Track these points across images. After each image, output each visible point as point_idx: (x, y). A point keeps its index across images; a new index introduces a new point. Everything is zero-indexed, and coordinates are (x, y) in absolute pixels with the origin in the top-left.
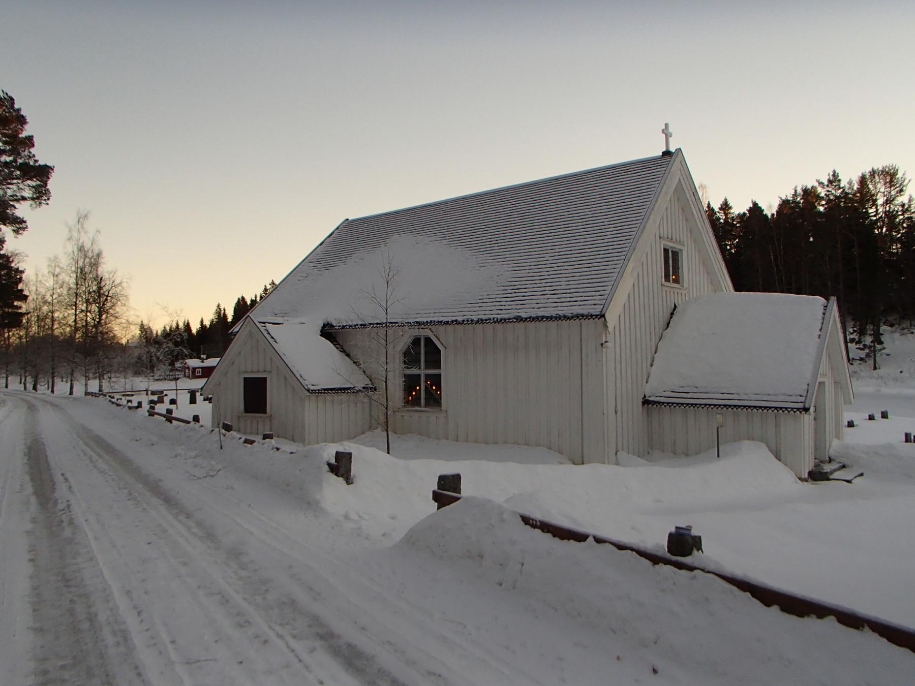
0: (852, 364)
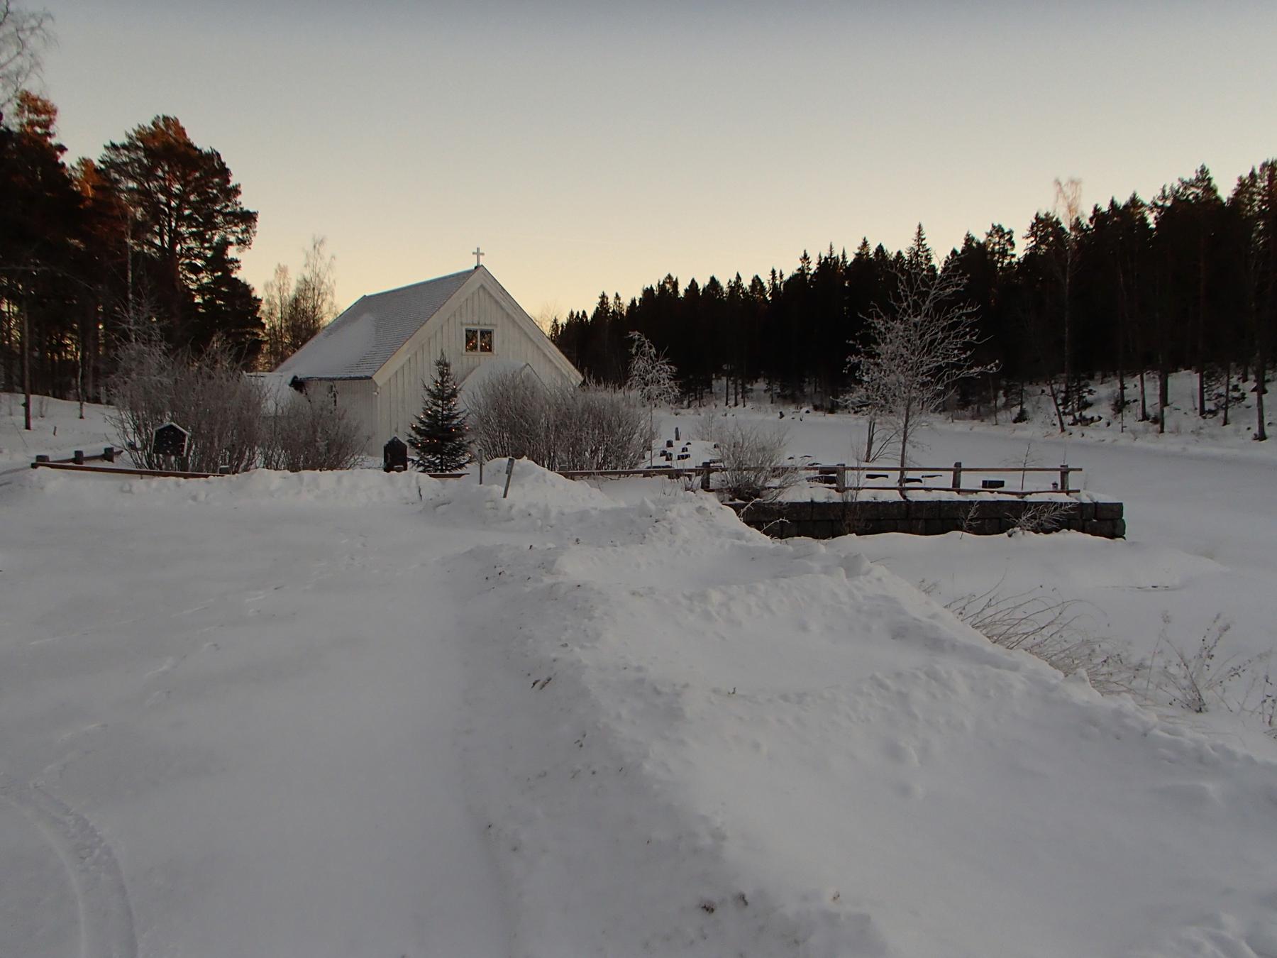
0: (1204, 418)
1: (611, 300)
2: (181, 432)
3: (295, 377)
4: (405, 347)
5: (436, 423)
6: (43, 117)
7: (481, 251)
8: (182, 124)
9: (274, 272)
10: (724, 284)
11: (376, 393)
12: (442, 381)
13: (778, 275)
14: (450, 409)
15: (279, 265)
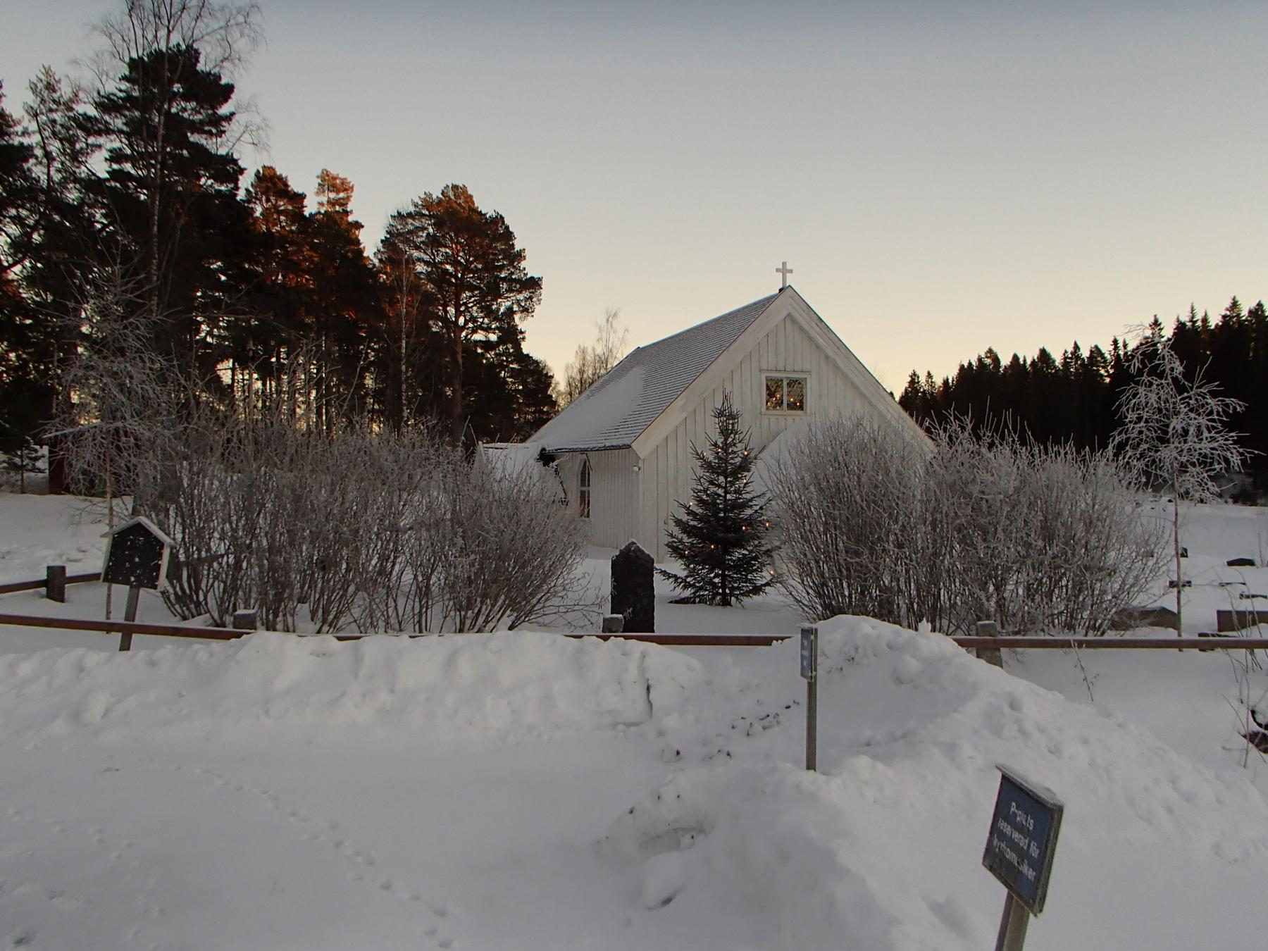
1: (923, 379)
2: (156, 539)
3: (543, 449)
4: (680, 402)
5: (715, 514)
6: (342, 195)
7: (788, 267)
9: (575, 353)
10: (1058, 359)
11: (636, 469)
12: (725, 443)
13: (1120, 344)
14: (738, 492)
15: (579, 347)
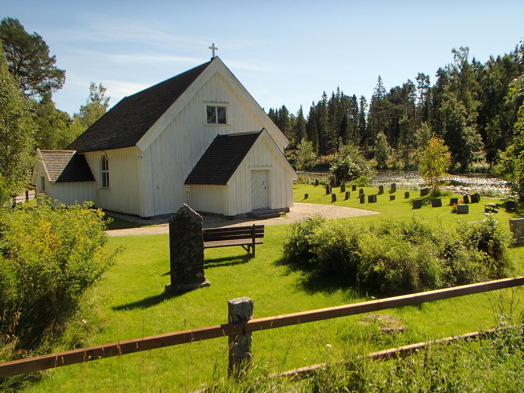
7: (215, 46)
8: (22, 23)
